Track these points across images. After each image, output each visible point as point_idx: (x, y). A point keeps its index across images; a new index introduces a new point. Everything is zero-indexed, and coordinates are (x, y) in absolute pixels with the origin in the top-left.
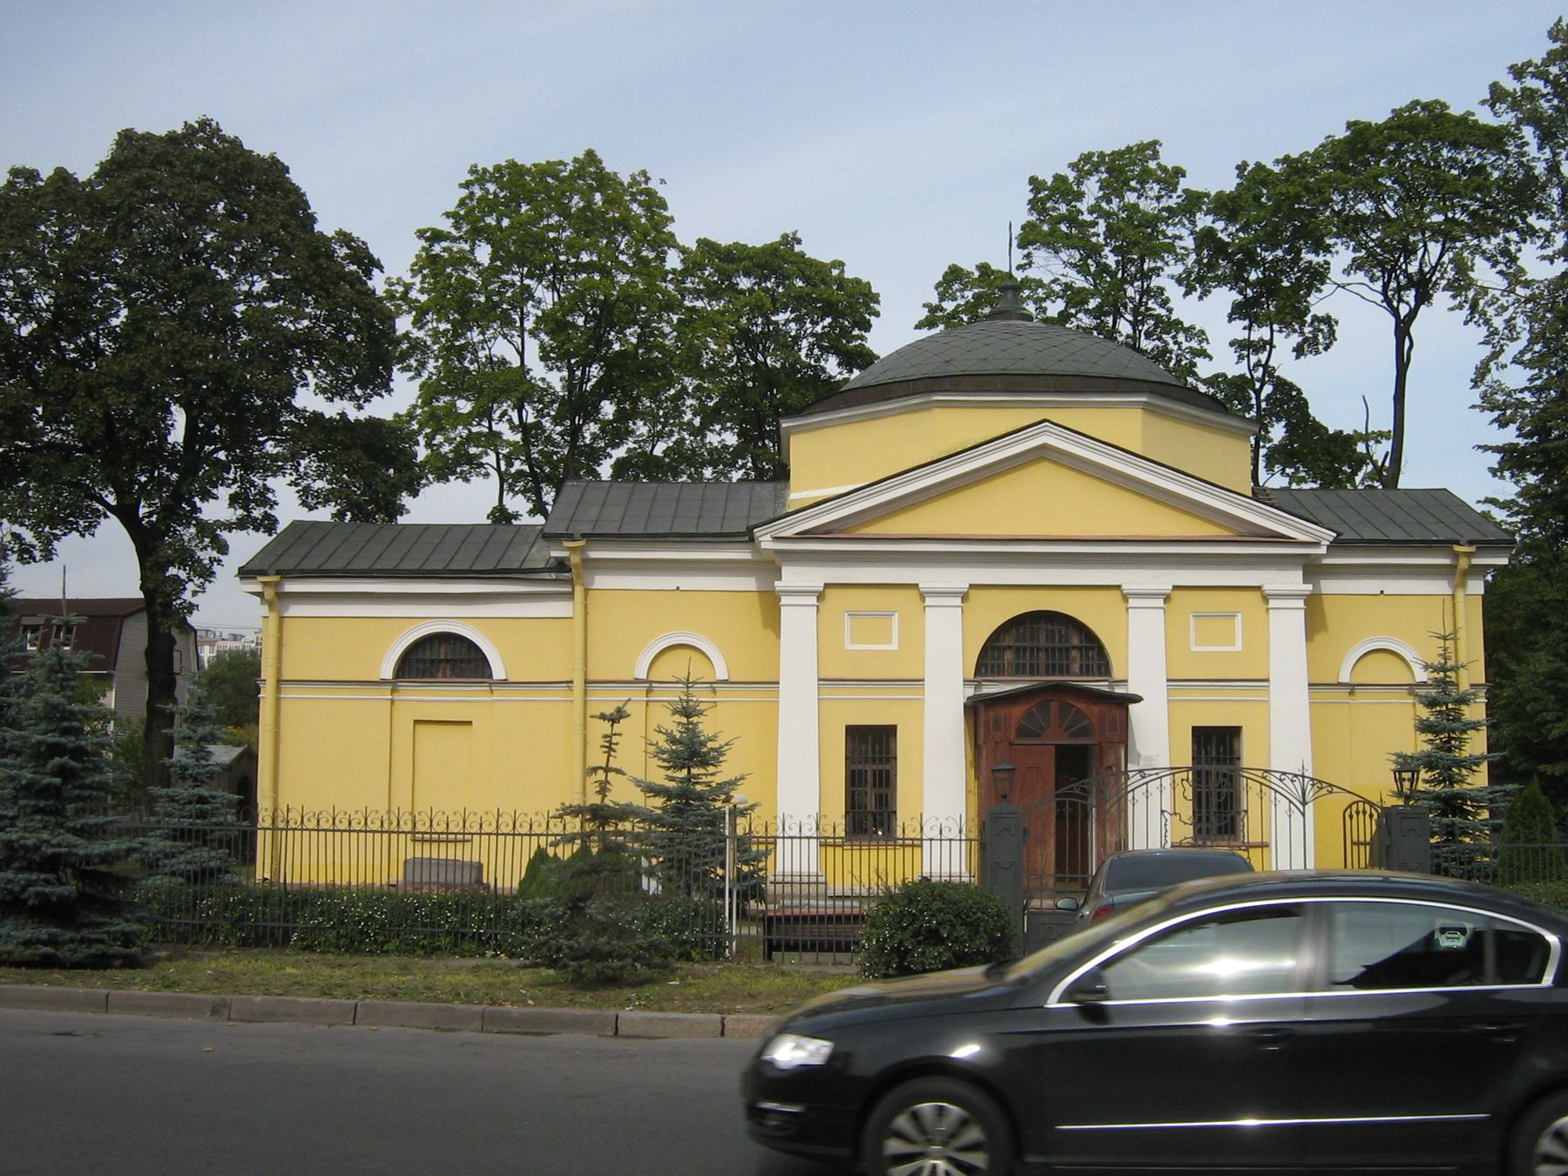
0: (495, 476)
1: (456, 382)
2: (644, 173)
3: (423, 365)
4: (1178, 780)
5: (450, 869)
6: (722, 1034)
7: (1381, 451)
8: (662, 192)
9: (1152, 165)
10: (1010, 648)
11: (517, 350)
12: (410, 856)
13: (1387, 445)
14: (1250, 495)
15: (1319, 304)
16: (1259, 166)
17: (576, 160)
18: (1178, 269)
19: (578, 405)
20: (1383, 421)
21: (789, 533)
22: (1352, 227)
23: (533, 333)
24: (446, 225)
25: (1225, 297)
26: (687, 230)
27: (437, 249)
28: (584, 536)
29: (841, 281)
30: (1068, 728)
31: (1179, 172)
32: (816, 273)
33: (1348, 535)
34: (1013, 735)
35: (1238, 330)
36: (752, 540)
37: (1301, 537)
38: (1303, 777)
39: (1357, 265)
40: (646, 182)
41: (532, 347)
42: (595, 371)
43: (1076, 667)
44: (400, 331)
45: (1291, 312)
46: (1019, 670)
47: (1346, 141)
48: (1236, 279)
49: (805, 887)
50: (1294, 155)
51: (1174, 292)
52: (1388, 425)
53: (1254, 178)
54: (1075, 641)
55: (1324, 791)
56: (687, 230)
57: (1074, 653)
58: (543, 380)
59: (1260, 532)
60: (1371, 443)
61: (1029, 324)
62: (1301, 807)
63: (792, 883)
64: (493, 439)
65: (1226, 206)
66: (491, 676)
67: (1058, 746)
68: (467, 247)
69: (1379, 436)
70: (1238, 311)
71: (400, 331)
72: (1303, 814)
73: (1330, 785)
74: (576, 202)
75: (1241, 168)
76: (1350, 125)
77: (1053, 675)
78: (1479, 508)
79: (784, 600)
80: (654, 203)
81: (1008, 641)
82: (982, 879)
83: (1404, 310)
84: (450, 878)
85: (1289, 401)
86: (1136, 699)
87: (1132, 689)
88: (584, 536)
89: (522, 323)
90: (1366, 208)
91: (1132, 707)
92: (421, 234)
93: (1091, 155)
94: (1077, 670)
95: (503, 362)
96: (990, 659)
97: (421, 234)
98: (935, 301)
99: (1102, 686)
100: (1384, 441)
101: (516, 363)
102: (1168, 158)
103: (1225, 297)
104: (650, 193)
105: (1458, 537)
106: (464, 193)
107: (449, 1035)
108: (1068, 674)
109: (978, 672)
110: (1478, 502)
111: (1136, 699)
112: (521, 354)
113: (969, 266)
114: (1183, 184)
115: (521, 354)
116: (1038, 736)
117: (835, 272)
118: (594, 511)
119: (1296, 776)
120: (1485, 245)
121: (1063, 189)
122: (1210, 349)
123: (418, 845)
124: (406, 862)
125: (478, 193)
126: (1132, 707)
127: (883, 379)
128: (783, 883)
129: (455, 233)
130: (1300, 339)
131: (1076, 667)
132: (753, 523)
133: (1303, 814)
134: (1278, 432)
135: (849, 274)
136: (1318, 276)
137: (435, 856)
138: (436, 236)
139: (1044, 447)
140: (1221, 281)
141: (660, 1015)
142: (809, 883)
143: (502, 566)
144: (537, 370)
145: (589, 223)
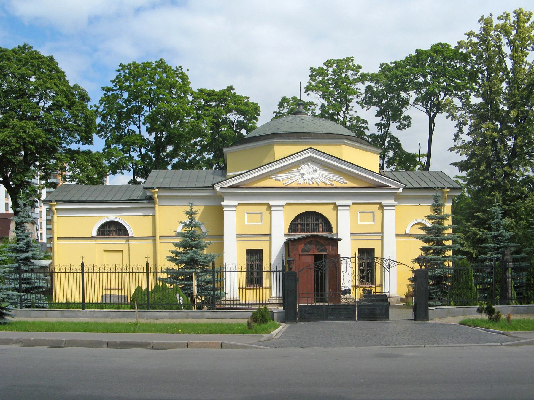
0: (132, 170)
1: (119, 139)
2: (180, 67)
3: (106, 133)
4: (348, 262)
5: (112, 298)
6: (188, 347)
7: (424, 160)
8: (187, 73)
9: (351, 64)
10: (300, 224)
11: (138, 127)
12: (104, 294)
13: (425, 158)
14: (378, 173)
15: (406, 112)
16: (387, 65)
17: (156, 62)
18: (359, 100)
19: (159, 146)
20: (425, 151)
21: (226, 186)
22: (418, 87)
23: (144, 124)
24: (111, 85)
25: (374, 109)
26: (195, 86)
27: (110, 94)
28: (158, 188)
29: (246, 104)
30: (318, 250)
31: (359, 67)
32: (238, 100)
33: (409, 185)
34: (300, 251)
35: (379, 120)
36: (214, 189)
37: (394, 187)
38: (389, 260)
39: (417, 100)
40: (181, 70)
41: (143, 128)
42: (165, 134)
43: (321, 229)
44: (97, 123)
45: (396, 115)
46: (303, 231)
47: (415, 56)
48: (378, 104)
49: (229, 302)
50: (398, 61)
51: (358, 107)
52: (426, 152)
53: (385, 68)
54: (320, 221)
55: (396, 264)
56: (195, 86)
57: (320, 225)
58: (148, 139)
59: (379, 184)
60: (421, 158)
61: (306, 116)
62: (388, 270)
63: (231, 300)
64: (131, 158)
65: (373, 78)
66: (128, 235)
67: (314, 255)
68: (119, 93)
69: (423, 155)
70: (379, 114)
71: (97, 123)
72: (389, 272)
73: (398, 262)
74: (157, 77)
75: (382, 65)
76: (417, 51)
77: (314, 232)
78: (454, 179)
79: (225, 209)
80: (184, 78)
81: (298, 221)
82: (345, 305)
83: (432, 114)
84: (120, 301)
85: (396, 144)
86: (340, 240)
87: (339, 237)
88: (158, 188)
89: (139, 118)
90: (421, 80)
91: (339, 242)
92: (103, 89)
93: (331, 60)
94: (322, 231)
95: (133, 132)
96: (293, 226)
97: (103, 89)
98: (278, 111)
99: (328, 235)
100: (424, 157)
101: (137, 132)
102: (356, 62)
103: (374, 109)
104: (183, 74)
105: (444, 186)
106: (118, 73)
107: (207, 349)
108: (319, 232)
109: (289, 231)
110: (454, 178)
111: (340, 240)
112: (139, 128)
113: (289, 97)
114: (361, 71)
115: (139, 128)
116: (308, 252)
117: (246, 101)
118: (161, 180)
119: (387, 259)
120: (459, 93)
121: (321, 72)
122: (369, 126)
123: (107, 291)
124: (102, 296)
125: (123, 74)
126: (339, 242)
127: (257, 134)
128: (228, 300)
129: (114, 88)
130: (399, 124)
131: (321, 229)
132: (214, 183)
133: (389, 272)
134: (391, 154)
135: (251, 101)
136: (405, 103)
137: (117, 294)
138: (108, 90)
139: (310, 157)
140: (374, 104)
141: (213, 341)
142: (233, 300)
143: (131, 198)
144: (145, 135)
145: (161, 84)
